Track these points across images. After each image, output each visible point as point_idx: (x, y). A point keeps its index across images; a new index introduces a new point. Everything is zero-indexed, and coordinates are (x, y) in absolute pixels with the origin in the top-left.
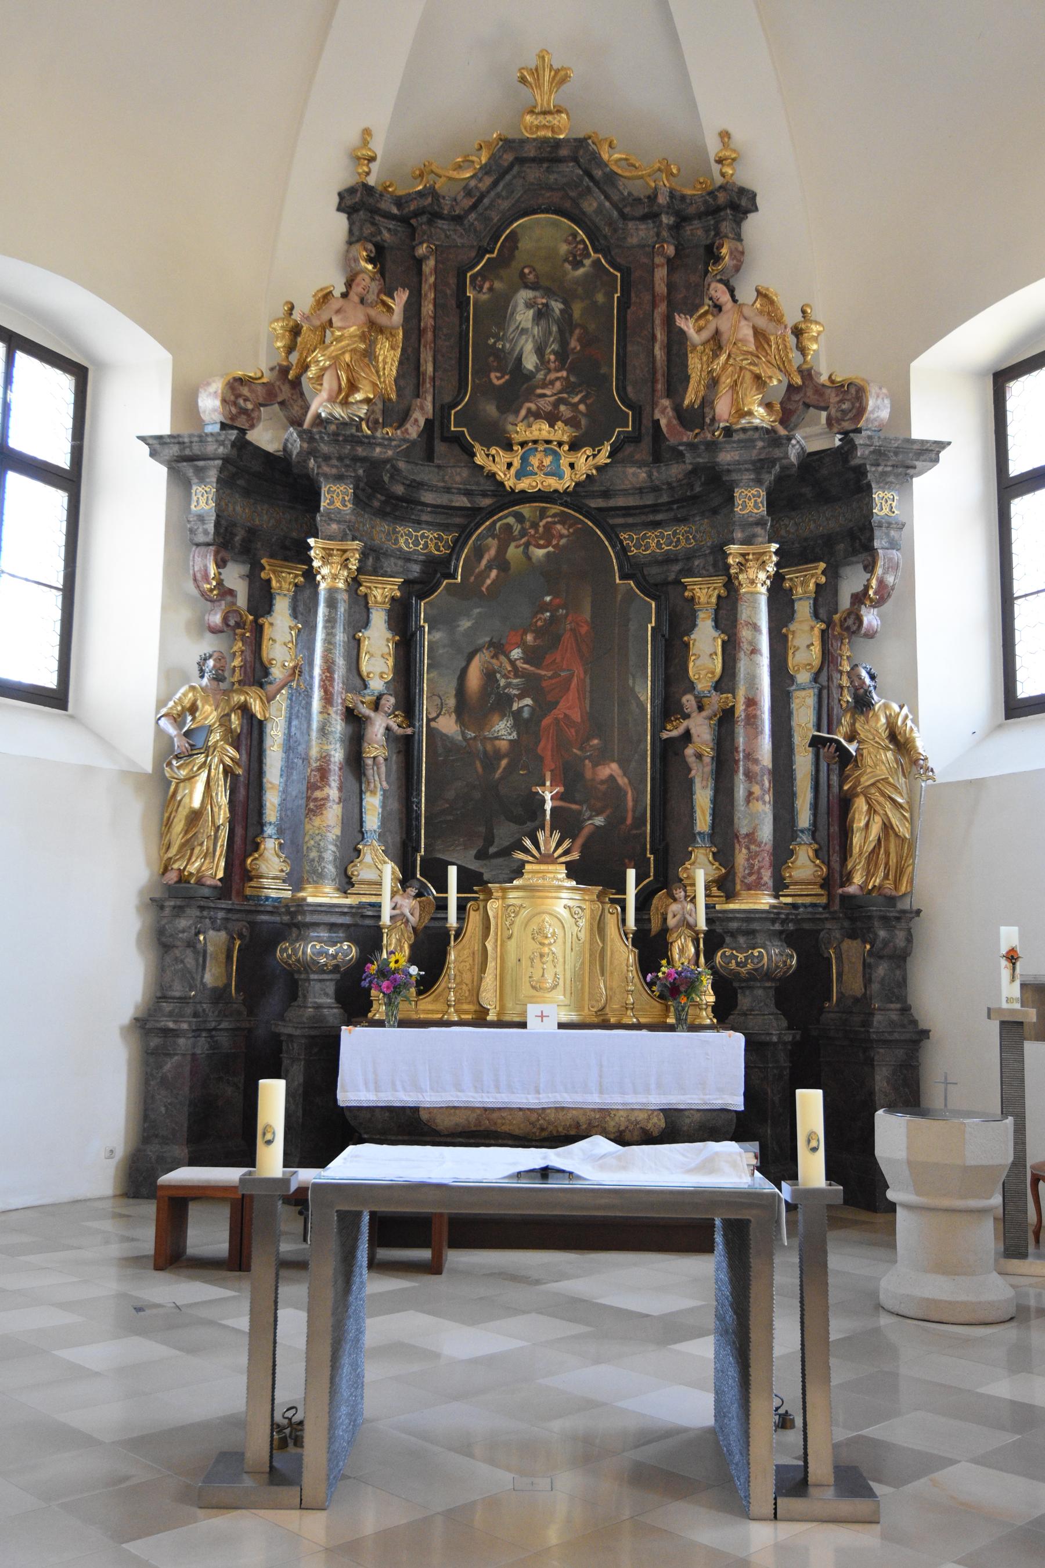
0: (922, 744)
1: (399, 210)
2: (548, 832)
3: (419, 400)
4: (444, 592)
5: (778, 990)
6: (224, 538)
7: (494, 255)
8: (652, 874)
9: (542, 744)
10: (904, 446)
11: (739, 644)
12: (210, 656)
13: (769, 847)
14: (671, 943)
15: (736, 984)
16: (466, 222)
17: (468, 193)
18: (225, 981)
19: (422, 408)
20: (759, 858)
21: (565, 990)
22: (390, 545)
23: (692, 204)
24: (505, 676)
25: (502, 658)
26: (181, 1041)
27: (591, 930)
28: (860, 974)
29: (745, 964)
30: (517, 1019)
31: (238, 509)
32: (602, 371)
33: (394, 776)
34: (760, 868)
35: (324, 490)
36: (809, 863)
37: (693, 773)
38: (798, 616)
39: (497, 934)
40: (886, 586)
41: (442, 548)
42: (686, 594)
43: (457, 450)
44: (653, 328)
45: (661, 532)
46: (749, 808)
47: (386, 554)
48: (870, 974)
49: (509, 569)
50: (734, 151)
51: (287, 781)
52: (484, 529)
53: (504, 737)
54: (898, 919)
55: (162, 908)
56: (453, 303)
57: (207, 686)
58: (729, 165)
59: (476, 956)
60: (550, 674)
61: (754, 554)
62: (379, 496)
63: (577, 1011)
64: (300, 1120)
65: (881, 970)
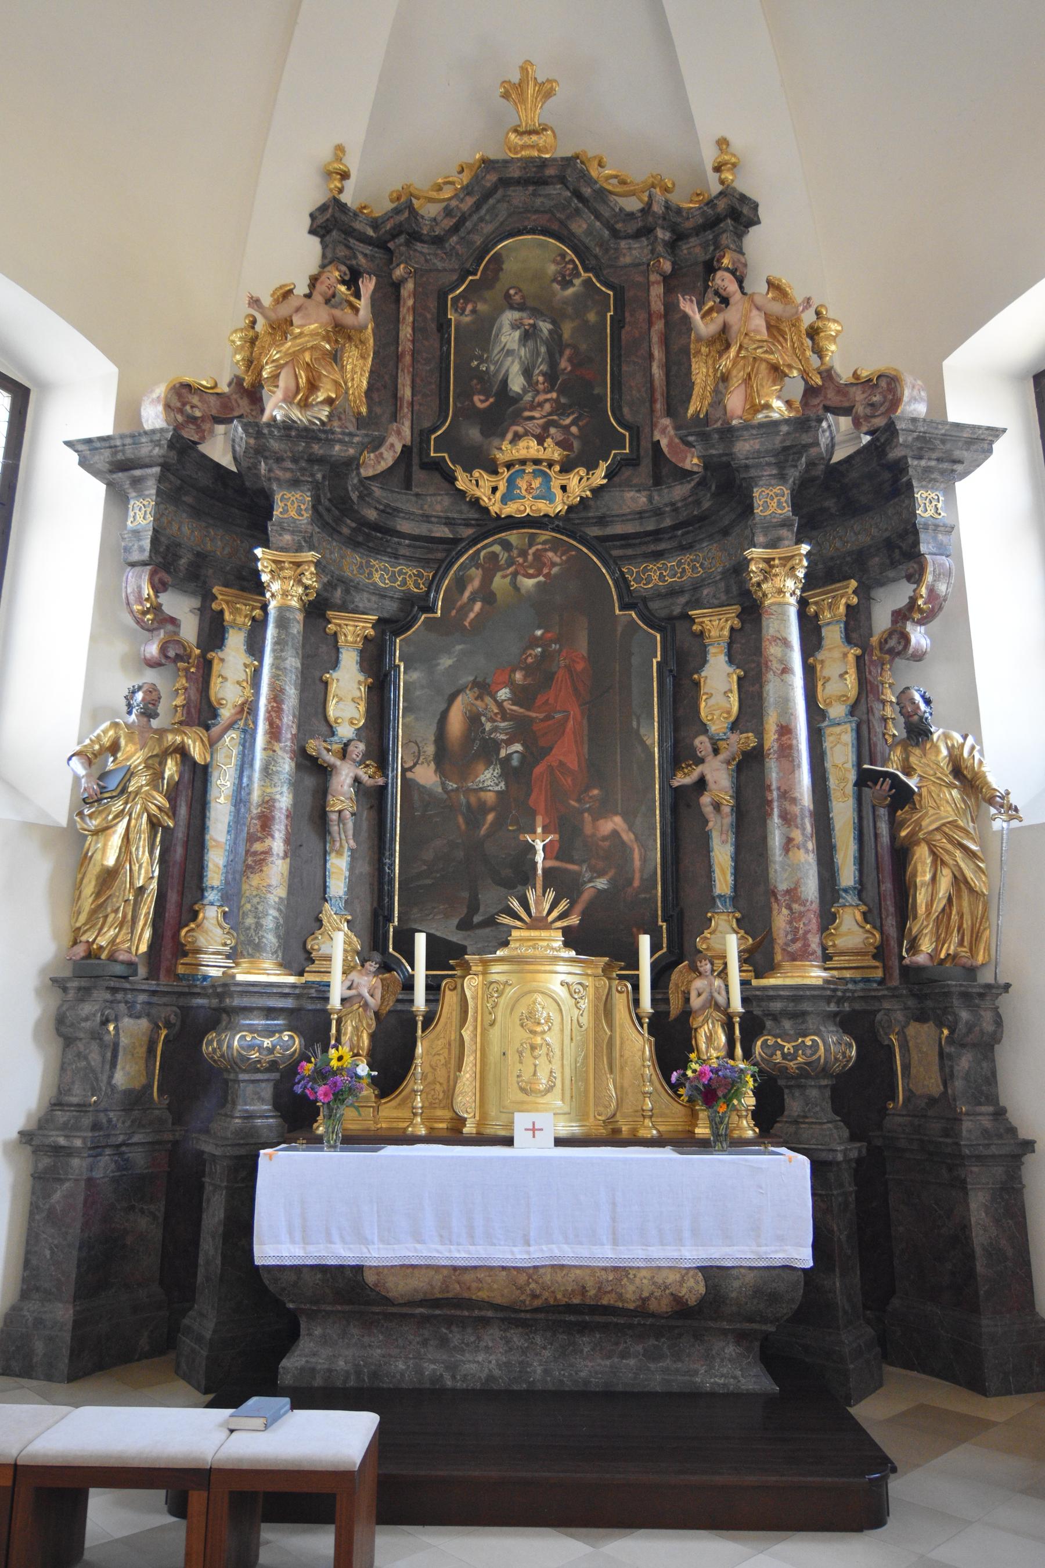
0: (996, 778)
1: (375, 232)
3: (395, 424)
5: (834, 1089)
6: (164, 558)
7: (477, 277)
8: (665, 945)
9: (533, 796)
10: (954, 434)
11: (766, 664)
12: (140, 688)
13: (815, 906)
14: (696, 1030)
15: (781, 1082)
16: (447, 245)
17: (448, 212)
18: (143, 1080)
19: (399, 433)
20: (804, 920)
21: (563, 1094)
22: (363, 579)
23: (688, 219)
25: (488, 700)
26: (75, 1162)
27: (596, 1013)
28: (936, 1068)
29: (794, 1057)
30: (502, 1133)
31: (186, 530)
32: (596, 392)
33: (364, 834)
34: (806, 933)
35: (277, 497)
36: (856, 928)
37: (711, 824)
38: (826, 643)
39: (476, 1020)
40: (937, 597)
42: (694, 628)
43: (437, 478)
47: (357, 588)
48: (952, 1067)
49: (495, 601)
50: (734, 155)
51: (236, 839)
54: (982, 996)
55: (65, 990)
56: (433, 326)
57: (134, 722)
58: (728, 170)
60: (541, 716)
61: (780, 559)
62: (349, 521)
63: (580, 1120)
64: (219, 1272)
65: (965, 1062)
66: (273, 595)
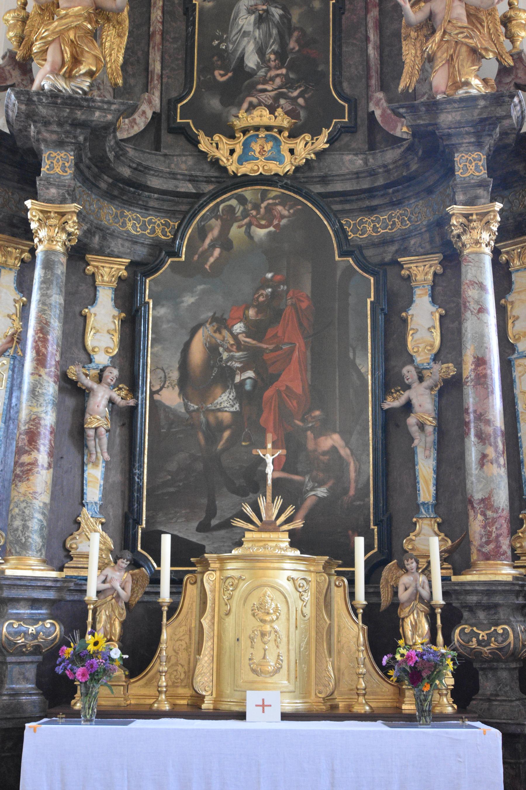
2: (269, 498)
4: (169, 270)
8: (376, 546)
9: (264, 415)
13: (506, 513)
14: (403, 619)
15: (476, 665)
19: (150, 102)
20: (497, 525)
21: (289, 675)
22: (117, 227)
24: (227, 350)
25: (225, 332)
27: (318, 604)
29: (487, 643)
30: (236, 709)
32: (320, 69)
33: (117, 448)
34: (498, 536)
35: (45, 156)
37: (416, 442)
39: (213, 610)
41: (168, 234)
42: (403, 272)
43: (182, 141)
44: (366, 31)
45: (376, 217)
46: (483, 472)
47: (112, 235)
52: (208, 211)
53: (227, 409)
56: (180, 10)
59: (193, 634)
60: (271, 347)
62: (106, 177)
63: (303, 698)
66: (40, 241)
